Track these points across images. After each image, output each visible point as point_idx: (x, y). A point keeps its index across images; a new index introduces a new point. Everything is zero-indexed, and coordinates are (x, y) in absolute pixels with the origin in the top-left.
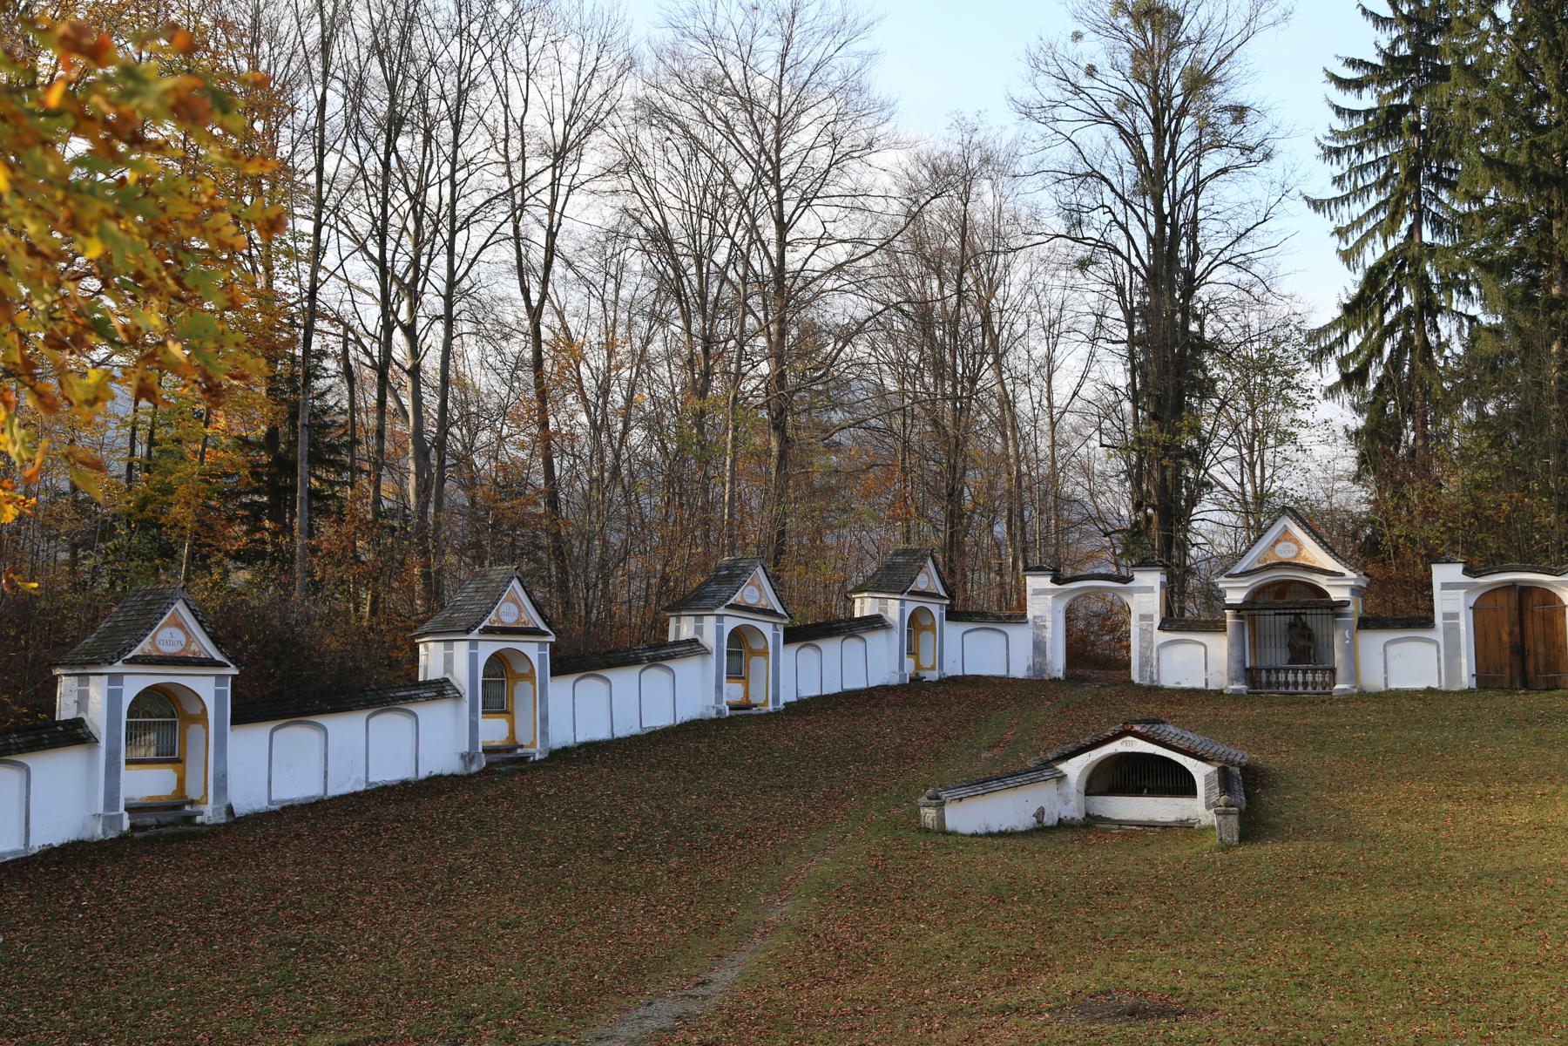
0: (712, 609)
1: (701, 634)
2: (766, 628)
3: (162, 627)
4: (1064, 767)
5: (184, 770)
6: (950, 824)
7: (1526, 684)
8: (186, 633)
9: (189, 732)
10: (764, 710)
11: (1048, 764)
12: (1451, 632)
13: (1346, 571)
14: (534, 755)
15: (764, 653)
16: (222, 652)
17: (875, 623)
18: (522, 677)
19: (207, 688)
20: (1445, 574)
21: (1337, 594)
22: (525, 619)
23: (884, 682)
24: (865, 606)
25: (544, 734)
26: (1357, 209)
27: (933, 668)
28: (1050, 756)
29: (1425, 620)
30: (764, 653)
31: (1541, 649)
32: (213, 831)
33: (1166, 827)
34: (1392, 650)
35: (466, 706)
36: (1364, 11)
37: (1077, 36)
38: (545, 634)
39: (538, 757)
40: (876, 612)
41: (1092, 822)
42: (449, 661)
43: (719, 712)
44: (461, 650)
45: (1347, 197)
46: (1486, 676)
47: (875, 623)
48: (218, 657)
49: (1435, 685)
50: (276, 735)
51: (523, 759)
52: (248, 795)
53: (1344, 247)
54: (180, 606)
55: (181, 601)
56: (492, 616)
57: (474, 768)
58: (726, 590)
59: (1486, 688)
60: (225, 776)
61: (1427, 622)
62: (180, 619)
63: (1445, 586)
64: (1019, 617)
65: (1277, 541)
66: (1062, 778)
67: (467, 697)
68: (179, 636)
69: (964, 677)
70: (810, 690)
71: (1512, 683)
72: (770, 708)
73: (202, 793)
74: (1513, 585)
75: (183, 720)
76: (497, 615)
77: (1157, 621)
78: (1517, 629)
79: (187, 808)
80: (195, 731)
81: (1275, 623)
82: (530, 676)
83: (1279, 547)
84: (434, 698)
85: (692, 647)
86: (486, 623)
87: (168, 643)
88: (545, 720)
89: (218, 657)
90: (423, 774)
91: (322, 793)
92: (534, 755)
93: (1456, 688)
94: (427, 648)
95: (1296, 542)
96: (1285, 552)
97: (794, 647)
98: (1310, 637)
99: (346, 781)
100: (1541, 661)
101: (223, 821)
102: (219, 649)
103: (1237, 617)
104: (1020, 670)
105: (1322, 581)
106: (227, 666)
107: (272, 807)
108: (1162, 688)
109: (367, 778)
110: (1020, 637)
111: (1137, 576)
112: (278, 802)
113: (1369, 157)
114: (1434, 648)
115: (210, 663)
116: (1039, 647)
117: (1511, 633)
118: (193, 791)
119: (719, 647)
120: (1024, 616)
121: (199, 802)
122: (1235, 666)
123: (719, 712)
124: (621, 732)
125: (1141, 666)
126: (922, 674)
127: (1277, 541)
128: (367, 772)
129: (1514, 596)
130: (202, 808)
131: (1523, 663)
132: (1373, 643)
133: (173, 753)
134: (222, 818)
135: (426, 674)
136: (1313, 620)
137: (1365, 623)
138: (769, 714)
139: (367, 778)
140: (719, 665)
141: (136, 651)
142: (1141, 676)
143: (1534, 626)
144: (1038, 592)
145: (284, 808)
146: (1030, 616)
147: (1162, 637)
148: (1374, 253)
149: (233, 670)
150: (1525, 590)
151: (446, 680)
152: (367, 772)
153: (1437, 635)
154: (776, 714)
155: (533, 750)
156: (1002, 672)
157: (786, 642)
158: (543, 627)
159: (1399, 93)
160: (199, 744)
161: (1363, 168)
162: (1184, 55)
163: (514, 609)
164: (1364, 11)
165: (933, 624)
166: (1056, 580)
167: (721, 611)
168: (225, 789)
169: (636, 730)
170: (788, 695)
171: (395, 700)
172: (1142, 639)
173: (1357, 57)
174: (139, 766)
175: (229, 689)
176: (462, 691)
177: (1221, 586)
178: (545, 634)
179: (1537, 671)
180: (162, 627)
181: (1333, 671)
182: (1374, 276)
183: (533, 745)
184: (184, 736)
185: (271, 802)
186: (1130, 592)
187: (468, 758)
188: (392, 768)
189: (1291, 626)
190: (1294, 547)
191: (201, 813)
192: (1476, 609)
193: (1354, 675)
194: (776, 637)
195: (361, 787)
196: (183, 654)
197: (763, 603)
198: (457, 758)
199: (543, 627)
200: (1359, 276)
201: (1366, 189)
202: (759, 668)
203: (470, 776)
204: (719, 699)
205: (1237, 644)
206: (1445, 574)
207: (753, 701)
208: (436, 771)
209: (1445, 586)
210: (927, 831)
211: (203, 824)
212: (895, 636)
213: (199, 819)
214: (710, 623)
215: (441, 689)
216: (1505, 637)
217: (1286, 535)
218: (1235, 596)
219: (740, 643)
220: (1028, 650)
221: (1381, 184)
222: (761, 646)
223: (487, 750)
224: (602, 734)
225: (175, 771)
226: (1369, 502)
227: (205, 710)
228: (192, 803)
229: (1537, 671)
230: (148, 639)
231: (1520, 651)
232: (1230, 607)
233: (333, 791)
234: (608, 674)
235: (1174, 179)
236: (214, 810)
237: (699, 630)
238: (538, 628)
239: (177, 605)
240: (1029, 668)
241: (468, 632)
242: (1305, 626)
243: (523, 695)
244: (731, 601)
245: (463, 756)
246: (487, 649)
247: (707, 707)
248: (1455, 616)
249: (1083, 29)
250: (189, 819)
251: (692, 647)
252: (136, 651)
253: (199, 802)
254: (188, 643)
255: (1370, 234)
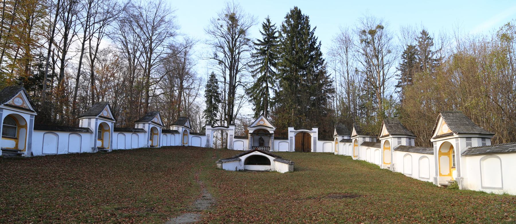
0: (148, 122)
1: (144, 128)
2: (158, 128)
3: (16, 97)
4: (241, 158)
5: (18, 142)
6: (224, 168)
7: (304, 151)
8: (23, 101)
9: (20, 131)
10: (157, 147)
11: (237, 157)
12: (291, 140)
13: (273, 127)
14: (109, 150)
15: (157, 134)
16: (33, 108)
17: (176, 132)
18: (106, 131)
19: (27, 117)
20: (291, 129)
21: (271, 132)
22: (109, 116)
23: (178, 145)
24: (174, 128)
25: (111, 145)
26: (256, 67)
27: (187, 143)
28: (238, 155)
29: (287, 138)
30: (157, 134)
31: (307, 144)
32: (27, 159)
33: (262, 172)
34: (280, 144)
35: (94, 135)
36: (260, 32)
37: (219, 19)
38: (113, 120)
39: (110, 151)
40: (176, 130)
41: (246, 170)
42: (89, 124)
43: (148, 146)
44: (93, 121)
45: (255, 65)
46: (297, 150)
47: (176, 132)
48: (32, 109)
49: (288, 151)
50: (45, 135)
51: (106, 151)
52: (37, 151)
53: (253, 74)
54: (22, 92)
55: (23, 90)
56: (101, 113)
57: (95, 152)
58: (151, 118)
59: (296, 152)
60: (31, 144)
61: (287, 139)
62: (21, 96)
63: (291, 132)
64: (204, 134)
65: (260, 121)
66: (240, 160)
67: (94, 133)
68: (21, 101)
69: (191, 146)
70: (165, 145)
71: (301, 150)
72: (158, 147)
73: (24, 148)
74: (302, 132)
75: (18, 127)
76: (102, 113)
77: (234, 136)
78: (303, 140)
79: (19, 152)
80: (22, 130)
81: (257, 137)
82: (109, 131)
83: (260, 122)
84: (86, 132)
85: (142, 131)
86: (100, 115)
87: (18, 102)
88: (112, 142)
89: (32, 109)
90: (82, 152)
91: (56, 153)
92: (109, 150)
93: (292, 151)
94: (82, 121)
95: (264, 121)
96: (261, 123)
97: (163, 134)
98: (264, 141)
99: (63, 151)
100: (307, 147)
101: (30, 156)
102: (32, 107)
103: (251, 136)
104: (203, 146)
105: (268, 129)
106: (34, 112)
107: (43, 155)
108: (234, 150)
109: (68, 151)
110: (204, 139)
111: (230, 127)
112: (44, 154)
113: (259, 58)
114: (288, 144)
115: (29, 110)
116: (208, 141)
117: (302, 141)
118: (20, 147)
119: (149, 131)
120: (205, 134)
121: (22, 151)
122: (250, 146)
123: (148, 146)
124: (127, 148)
125: (230, 145)
126: (184, 145)
127: (260, 121)
128: (68, 149)
129: (303, 134)
130: (24, 152)
131: (303, 147)
132: (277, 142)
133: (15, 136)
134: (30, 156)
135: (82, 125)
136: (265, 138)
137: (276, 138)
138: (158, 148)
139: (68, 151)
140: (148, 136)
141: (8, 103)
142: (230, 148)
143: (306, 139)
144: (208, 129)
145: (46, 156)
146: (206, 134)
147: (234, 140)
148: (259, 75)
149: (36, 114)
150: (304, 133)
151: (89, 128)
152: (68, 149)
153: (289, 141)
154: (159, 148)
155: (108, 149)
156: (200, 146)
157: (162, 132)
158: (113, 118)
159: (265, 47)
160: (23, 134)
161: (258, 60)
162: (239, 27)
163: (106, 113)
164: (260, 32)
165: (187, 134)
166: (212, 127)
167: (150, 122)
168: (31, 147)
169: (130, 148)
170: (161, 145)
171: (77, 131)
172: (230, 140)
173: (259, 39)
174: (4, 138)
175: (34, 119)
176: (93, 131)
177: (248, 129)
178: (113, 120)
179: (306, 149)
180: (16, 97)
181: (269, 147)
182: (259, 80)
183: (108, 148)
184: (18, 132)
185: (43, 154)
186: (228, 130)
187: (94, 149)
188: (74, 149)
189: (260, 139)
190: (263, 122)
191: (24, 154)
192: (295, 136)
193: (273, 148)
194: (160, 130)
195: (67, 153)
196: (21, 106)
197: (158, 122)
198: (91, 148)
199: (113, 118)
200: (256, 80)
201: (259, 64)
202: (155, 137)
203: (94, 153)
204: (148, 143)
205: (250, 141)
206: (291, 129)
207: (154, 145)
208: (85, 151)
209: (291, 132)
210: (219, 169)
211: (24, 157)
212: (147, 134)
213: (23, 155)
214: (147, 125)
215: (87, 130)
216: (301, 142)
217: (262, 120)
218: (251, 131)
219: (153, 131)
220: (206, 141)
221: (262, 63)
222: (156, 132)
223: (98, 148)
224: (123, 148)
225: (15, 141)
226: (465, 48)
227: (26, 124)
228: (20, 151)
229: (306, 149)
230: (11, 100)
231: (303, 144)
232: (250, 133)
233: (59, 153)
234: (125, 133)
235: (235, 51)
236: (27, 153)
237: (144, 127)
238: (30, 109)
239: (21, 92)
240: (205, 145)
241: (96, 116)
242: (262, 139)
243: (106, 135)
244: (152, 121)
245: (92, 148)
246: (100, 122)
247: (145, 145)
248: (292, 137)
249: (220, 19)
250: (20, 155)
251: (142, 131)
252: (8, 103)
253: (22, 151)
254: (23, 104)
255: (258, 72)
